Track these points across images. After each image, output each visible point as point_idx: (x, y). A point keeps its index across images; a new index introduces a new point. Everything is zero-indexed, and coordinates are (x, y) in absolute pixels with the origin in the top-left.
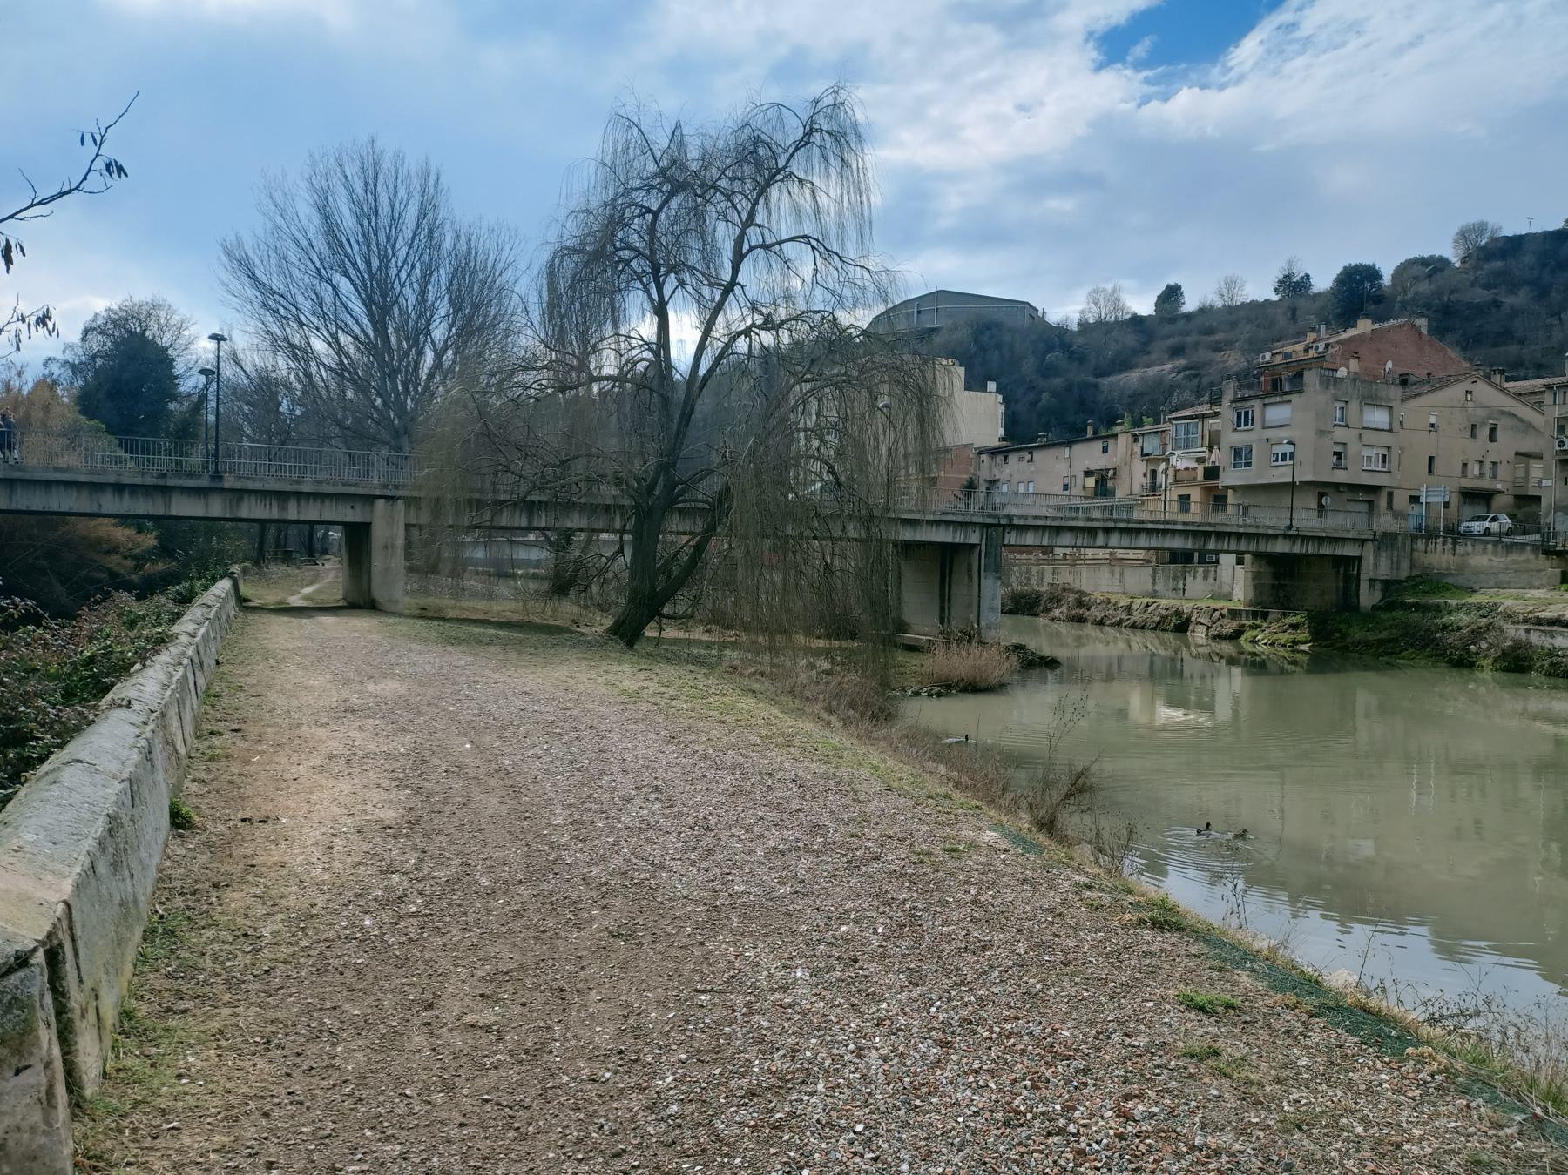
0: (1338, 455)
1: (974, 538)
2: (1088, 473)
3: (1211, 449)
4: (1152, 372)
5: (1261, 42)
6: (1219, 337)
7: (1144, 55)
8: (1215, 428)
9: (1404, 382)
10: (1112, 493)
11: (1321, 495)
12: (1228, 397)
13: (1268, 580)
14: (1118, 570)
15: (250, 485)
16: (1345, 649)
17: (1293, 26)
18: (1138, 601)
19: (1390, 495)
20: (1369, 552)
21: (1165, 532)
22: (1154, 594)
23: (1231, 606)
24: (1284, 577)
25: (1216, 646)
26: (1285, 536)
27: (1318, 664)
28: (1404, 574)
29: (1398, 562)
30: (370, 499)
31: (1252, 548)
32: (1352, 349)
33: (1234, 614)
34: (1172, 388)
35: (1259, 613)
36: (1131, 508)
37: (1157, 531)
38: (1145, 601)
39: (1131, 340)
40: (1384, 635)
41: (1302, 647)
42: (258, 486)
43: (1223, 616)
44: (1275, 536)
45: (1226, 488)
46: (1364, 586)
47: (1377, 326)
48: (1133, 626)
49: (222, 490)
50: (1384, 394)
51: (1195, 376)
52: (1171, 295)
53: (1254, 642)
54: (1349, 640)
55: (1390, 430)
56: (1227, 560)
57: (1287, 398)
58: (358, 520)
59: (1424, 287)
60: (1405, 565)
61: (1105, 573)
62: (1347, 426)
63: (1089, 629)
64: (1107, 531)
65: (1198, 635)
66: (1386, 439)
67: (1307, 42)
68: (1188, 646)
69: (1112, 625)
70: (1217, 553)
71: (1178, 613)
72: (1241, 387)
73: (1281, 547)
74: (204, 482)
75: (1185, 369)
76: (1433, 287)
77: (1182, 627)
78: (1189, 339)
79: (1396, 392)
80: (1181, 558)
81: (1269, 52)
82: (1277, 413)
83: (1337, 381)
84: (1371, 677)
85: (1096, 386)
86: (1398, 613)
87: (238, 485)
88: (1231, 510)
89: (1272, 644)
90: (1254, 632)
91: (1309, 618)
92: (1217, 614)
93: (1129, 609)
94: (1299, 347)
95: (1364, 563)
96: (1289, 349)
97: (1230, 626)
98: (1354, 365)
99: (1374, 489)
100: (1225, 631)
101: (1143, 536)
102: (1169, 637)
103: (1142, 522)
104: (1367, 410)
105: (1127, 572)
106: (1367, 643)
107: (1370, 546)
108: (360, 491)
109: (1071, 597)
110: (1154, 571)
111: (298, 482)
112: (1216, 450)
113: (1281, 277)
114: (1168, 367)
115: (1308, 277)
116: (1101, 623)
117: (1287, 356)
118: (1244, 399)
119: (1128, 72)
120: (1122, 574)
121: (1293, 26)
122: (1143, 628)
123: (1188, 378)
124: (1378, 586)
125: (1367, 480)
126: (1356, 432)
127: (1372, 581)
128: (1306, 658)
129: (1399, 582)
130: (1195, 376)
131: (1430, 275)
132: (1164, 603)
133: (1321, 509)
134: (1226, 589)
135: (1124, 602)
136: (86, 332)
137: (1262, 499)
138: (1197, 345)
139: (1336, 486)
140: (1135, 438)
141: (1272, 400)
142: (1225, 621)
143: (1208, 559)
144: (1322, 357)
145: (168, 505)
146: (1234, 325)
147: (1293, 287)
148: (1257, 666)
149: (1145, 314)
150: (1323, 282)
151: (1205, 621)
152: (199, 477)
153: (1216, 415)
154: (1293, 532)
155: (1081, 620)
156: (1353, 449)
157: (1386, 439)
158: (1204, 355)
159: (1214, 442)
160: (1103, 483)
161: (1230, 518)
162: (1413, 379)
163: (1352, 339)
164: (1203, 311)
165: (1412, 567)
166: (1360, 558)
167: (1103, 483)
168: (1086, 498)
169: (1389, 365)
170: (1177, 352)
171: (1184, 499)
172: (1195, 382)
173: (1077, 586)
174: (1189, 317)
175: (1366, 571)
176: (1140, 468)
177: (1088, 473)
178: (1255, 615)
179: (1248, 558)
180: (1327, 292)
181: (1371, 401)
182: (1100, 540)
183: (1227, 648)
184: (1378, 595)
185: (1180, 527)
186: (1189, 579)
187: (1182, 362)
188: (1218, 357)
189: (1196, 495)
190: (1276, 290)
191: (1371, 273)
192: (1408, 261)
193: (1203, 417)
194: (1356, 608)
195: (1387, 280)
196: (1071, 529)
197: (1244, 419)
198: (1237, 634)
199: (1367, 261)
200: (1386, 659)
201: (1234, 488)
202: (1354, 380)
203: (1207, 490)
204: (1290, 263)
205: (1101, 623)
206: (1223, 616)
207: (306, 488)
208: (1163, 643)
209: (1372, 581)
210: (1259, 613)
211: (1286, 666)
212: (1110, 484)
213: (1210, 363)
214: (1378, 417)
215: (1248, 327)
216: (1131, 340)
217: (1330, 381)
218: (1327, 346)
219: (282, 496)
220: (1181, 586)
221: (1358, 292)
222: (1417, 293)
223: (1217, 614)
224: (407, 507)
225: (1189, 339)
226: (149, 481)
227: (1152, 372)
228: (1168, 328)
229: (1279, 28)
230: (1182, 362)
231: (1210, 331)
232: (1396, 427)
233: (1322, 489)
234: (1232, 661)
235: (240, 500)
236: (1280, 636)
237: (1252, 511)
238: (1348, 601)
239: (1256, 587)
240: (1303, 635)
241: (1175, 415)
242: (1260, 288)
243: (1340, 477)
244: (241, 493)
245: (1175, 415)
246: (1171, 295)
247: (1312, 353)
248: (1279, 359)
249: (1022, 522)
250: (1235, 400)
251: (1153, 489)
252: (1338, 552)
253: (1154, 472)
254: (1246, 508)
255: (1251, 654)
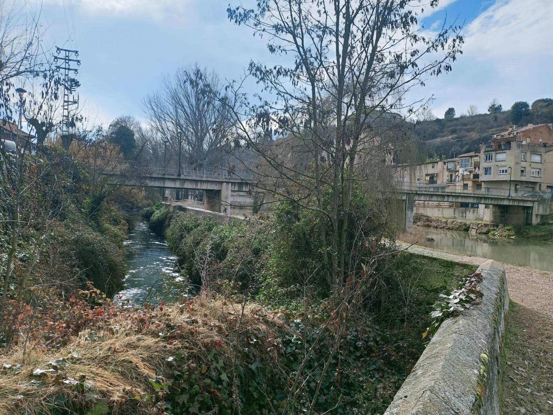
0: (522, 171)
1: (404, 198)
2: (427, 175)
3: (475, 168)
4: (445, 139)
5: (480, 23)
6: (469, 127)
7: (437, 27)
8: (476, 161)
9: (545, 145)
10: (436, 182)
11: (516, 185)
12: (483, 150)
13: (498, 214)
14: (441, 209)
15: (188, 178)
16: (529, 238)
17: (491, 17)
18: (450, 220)
19: (540, 185)
20: (536, 205)
21: (467, 197)
22: (455, 218)
23: (483, 223)
24: (504, 212)
25: (480, 236)
26: (507, 199)
27: (517, 243)
28: (548, 213)
29: (546, 209)
30: (221, 183)
31: (493, 203)
32: (526, 134)
33: (486, 225)
34: (452, 145)
35: (495, 225)
36: (443, 188)
37: (465, 196)
38: (452, 220)
39: (436, 127)
40: (543, 233)
41: (512, 237)
42: (190, 178)
43: (482, 226)
44: (504, 199)
45: (482, 182)
46: (534, 217)
47: (534, 126)
48: (449, 229)
49: (180, 179)
50: (539, 150)
51: (461, 141)
52: (451, 111)
53: (494, 235)
54: (530, 235)
55: (541, 163)
56: (482, 207)
57: (504, 151)
58: (217, 189)
59: (545, 110)
60: (548, 210)
61: (436, 209)
62: (526, 161)
63: (432, 230)
64: (448, 196)
65: (473, 232)
66: (539, 166)
67: (497, 22)
68: (469, 236)
69: (441, 228)
70: (478, 204)
71: (465, 225)
72: (487, 147)
73: (506, 203)
74: (175, 177)
75: (457, 138)
76: (548, 110)
77: (467, 229)
78: (458, 128)
79: (542, 150)
80: (465, 205)
81: (482, 26)
82: (501, 156)
83: (523, 146)
84: (538, 248)
85: (424, 144)
86: (546, 226)
87: (185, 178)
88: (483, 190)
89: (501, 236)
90: (494, 232)
91: (514, 227)
92: (480, 225)
93: (446, 223)
94: (506, 133)
95: (534, 209)
96: (503, 134)
97: (485, 230)
98: (528, 140)
99: (535, 183)
100: (483, 231)
101: (460, 198)
102: (462, 233)
103: (460, 193)
104: (532, 155)
105: (444, 210)
106: (536, 236)
107: (536, 203)
108: (219, 180)
109: (425, 218)
110: (455, 210)
111: (202, 177)
112: (477, 169)
113: (491, 106)
114: (450, 137)
115: (500, 106)
116: (436, 227)
117: (502, 136)
118: (488, 151)
119: (431, 33)
120: (442, 211)
121: (491, 17)
122: (452, 229)
123: (458, 141)
124: (539, 217)
125: (532, 180)
126: (529, 163)
127: (537, 215)
128: (513, 241)
129: (547, 216)
130: (461, 141)
131: (547, 106)
132: (459, 221)
133: (516, 190)
134: (481, 217)
135: (444, 220)
136: (110, 126)
137: (494, 186)
138: (461, 129)
139: (522, 182)
140: (445, 163)
141: (499, 152)
142: (483, 228)
143: (475, 206)
144: (515, 137)
145: (164, 184)
146: (474, 123)
147: (495, 109)
148: (494, 243)
149: (441, 118)
150: (507, 107)
151: (476, 228)
152: (174, 175)
153: (476, 156)
154: (510, 198)
155: (429, 226)
156: (528, 169)
157: (539, 166)
158: (463, 133)
159: (477, 165)
160: (432, 178)
161: (483, 191)
162: (548, 145)
163: (526, 131)
164: (462, 117)
165: (550, 211)
166: (532, 207)
167: (432, 178)
168: (426, 184)
169: (541, 140)
170: (453, 132)
171: (465, 186)
172: (460, 143)
173: (425, 214)
174: (457, 119)
175: (535, 211)
176: (446, 174)
177: (427, 175)
178: (494, 226)
179: (491, 206)
180: (508, 111)
181: (534, 152)
182: (446, 200)
183: (484, 237)
184: (539, 220)
185: (473, 195)
186: (468, 213)
187: (455, 136)
188: (468, 134)
189: (470, 184)
190: (489, 110)
191: (525, 105)
192: (538, 100)
193: (471, 157)
194: (530, 224)
195: (530, 108)
196: (436, 195)
197: (488, 158)
198: (487, 233)
199: (524, 101)
200: (543, 242)
201: (484, 182)
202: (529, 145)
203: (474, 182)
204: (494, 100)
205: (436, 227)
206: (482, 226)
207: (204, 179)
208: (460, 235)
209: (537, 215)
210: (495, 225)
211: (505, 243)
212: (435, 179)
213: (466, 136)
214: (537, 158)
215: (480, 124)
216: (436, 127)
217: (520, 146)
218: (517, 133)
219: (196, 181)
220: (464, 215)
221: (520, 113)
222: (542, 112)
223: (480, 225)
224: (232, 185)
225: (458, 128)
226: (160, 176)
227: (445, 139)
228: (450, 123)
229: (486, 17)
230: (455, 136)
231: (465, 125)
232: (543, 162)
233: (516, 183)
234: (485, 241)
235: (184, 182)
236: (503, 233)
237: (491, 190)
238: (528, 222)
239: (494, 216)
240: (512, 233)
241: (461, 156)
242: (483, 110)
243: (523, 179)
244: (185, 180)
245: (461, 156)
246: (451, 111)
247: (512, 135)
248: (499, 137)
249: (420, 193)
250: (485, 152)
251: (451, 181)
252: (525, 205)
253: (451, 175)
254: (488, 189)
255: (492, 239)
